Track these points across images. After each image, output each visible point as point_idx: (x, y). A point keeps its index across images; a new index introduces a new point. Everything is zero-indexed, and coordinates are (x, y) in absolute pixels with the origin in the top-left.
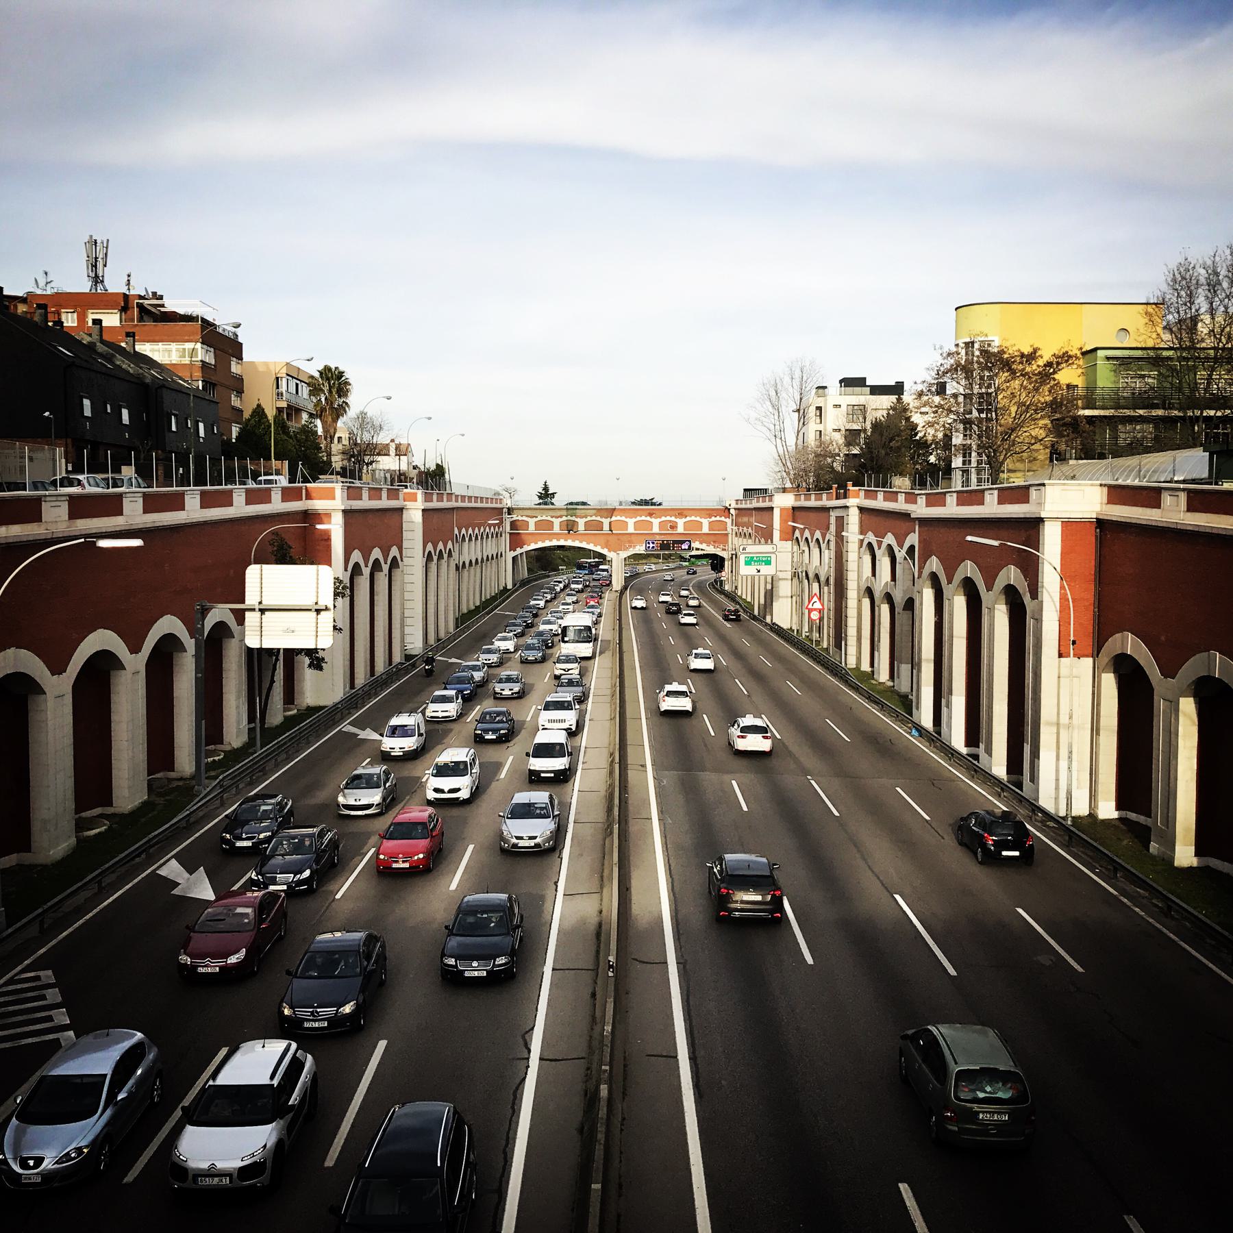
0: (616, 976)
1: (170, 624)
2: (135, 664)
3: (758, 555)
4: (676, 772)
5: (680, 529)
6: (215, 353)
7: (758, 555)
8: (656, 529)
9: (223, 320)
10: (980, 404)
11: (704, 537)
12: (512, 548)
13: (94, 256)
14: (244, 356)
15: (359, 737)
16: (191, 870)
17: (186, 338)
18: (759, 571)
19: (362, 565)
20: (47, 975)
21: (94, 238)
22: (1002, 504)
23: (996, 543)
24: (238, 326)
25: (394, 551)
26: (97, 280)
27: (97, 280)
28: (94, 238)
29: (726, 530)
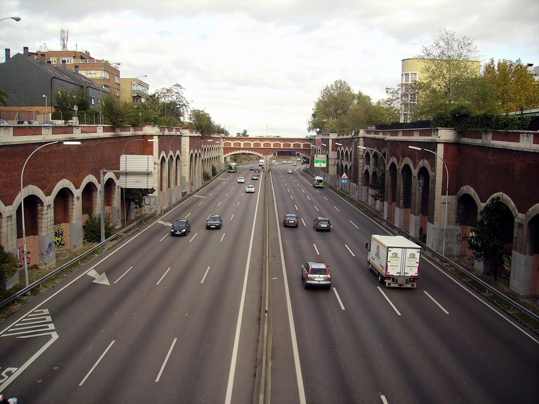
0: (268, 316)
1: (90, 178)
2: (78, 193)
3: (321, 159)
4: (290, 240)
5: (292, 147)
6: (109, 74)
7: (321, 159)
8: (282, 147)
9: (112, 61)
10: (411, 98)
11: (301, 150)
12: (224, 154)
13: (63, 37)
14: (120, 76)
15: (164, 225)
16: (100, 274)
17: (98, 68)
18: (320, 165)
19: (165, 157)
20: (46, 311)
21: (63, 30)
22: (392, 163)
23: (420, 149)
24: (119, 64)
25: (178, 152)
26: (64, 46)
27: (64, 46)
28: (63, 30)
29: (310, 148)
